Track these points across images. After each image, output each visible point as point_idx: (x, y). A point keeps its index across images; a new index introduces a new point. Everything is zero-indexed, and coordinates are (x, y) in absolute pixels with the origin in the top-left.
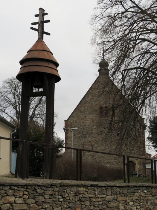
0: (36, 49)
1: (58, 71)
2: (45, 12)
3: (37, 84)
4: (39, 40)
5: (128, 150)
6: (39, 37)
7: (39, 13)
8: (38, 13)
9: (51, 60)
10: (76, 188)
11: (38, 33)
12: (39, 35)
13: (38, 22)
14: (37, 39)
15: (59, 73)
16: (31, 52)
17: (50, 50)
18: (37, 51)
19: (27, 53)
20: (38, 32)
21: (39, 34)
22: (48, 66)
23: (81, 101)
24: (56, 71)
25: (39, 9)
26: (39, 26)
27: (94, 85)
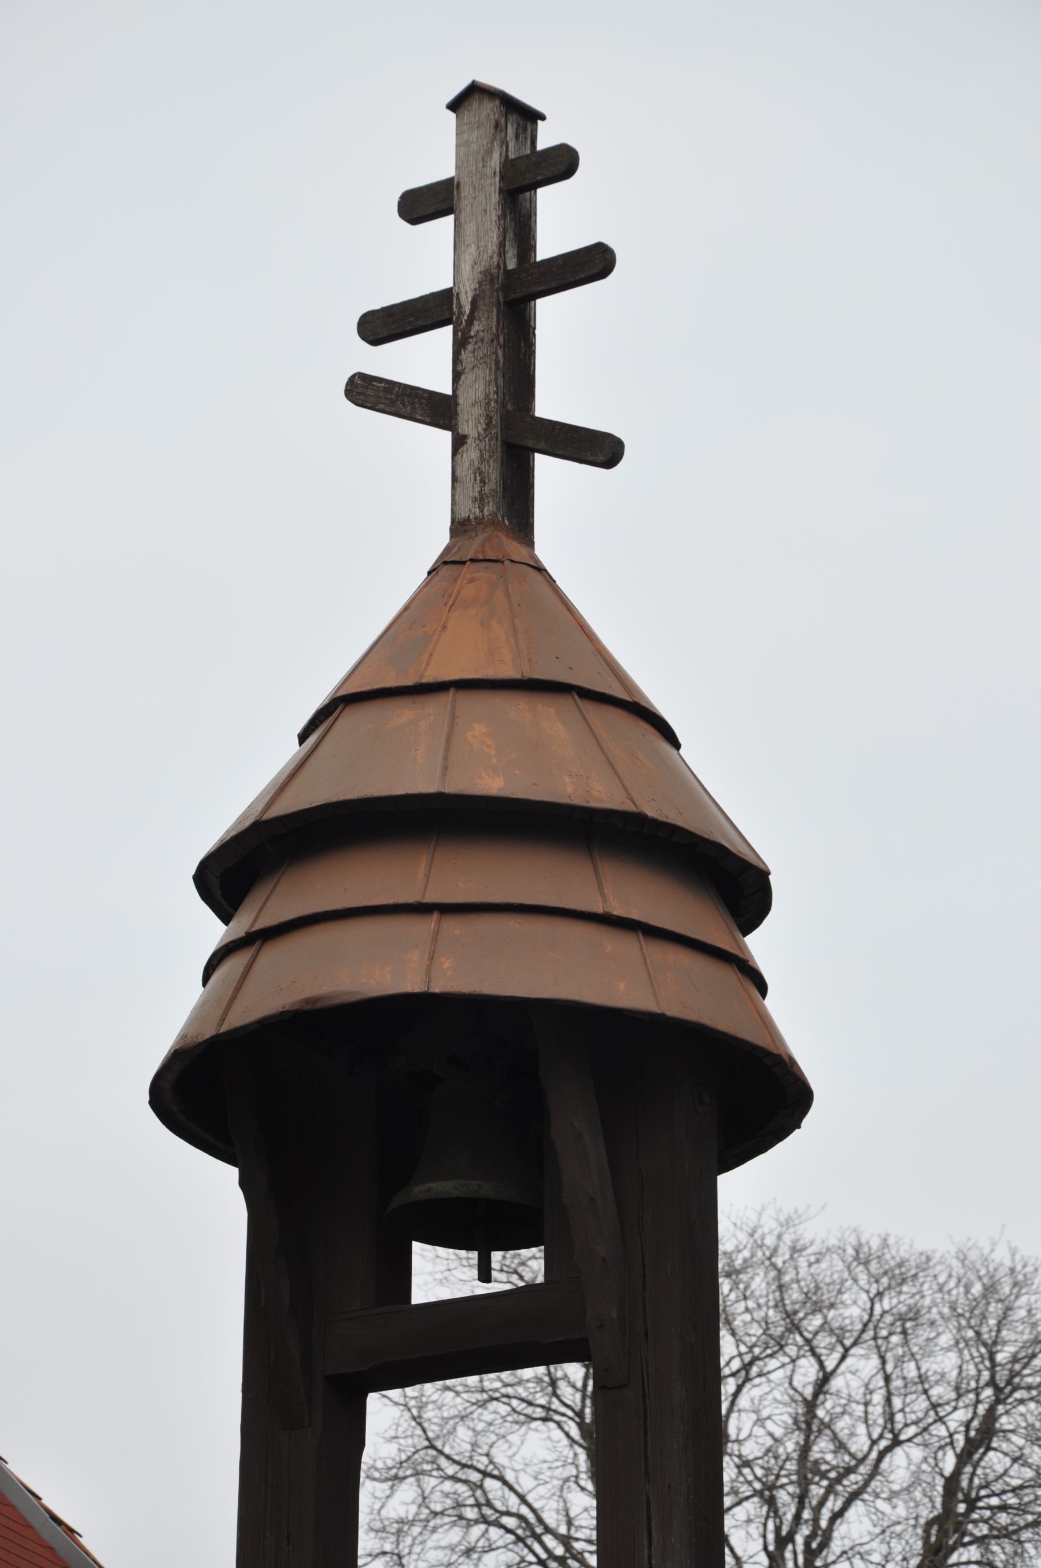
0: (410, 682)
1: (762, 988)
2: (546, 137)
3: (444, 1188)
4: (472, 548)
5: (397, 389)
6: (463, 514)
7: (456, 174)
8: (441, 279)
9: (639, 820)
10: (471, 482)
11: (459, 443)
12: (464, 472)
13: (445, 297)
14: (441, 539)
15: (771, 1003)
16: (349, 720)
17: (767, 867)
18: (435, 707)
19: (303, 738)
20: (444, 438)
21: (471, 454)
22: (599, 909)
23: (551, 582)
24: (729, 976)
25: (454, 106)
26: (459, 345)
27: (419, 417)
